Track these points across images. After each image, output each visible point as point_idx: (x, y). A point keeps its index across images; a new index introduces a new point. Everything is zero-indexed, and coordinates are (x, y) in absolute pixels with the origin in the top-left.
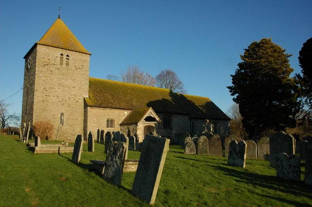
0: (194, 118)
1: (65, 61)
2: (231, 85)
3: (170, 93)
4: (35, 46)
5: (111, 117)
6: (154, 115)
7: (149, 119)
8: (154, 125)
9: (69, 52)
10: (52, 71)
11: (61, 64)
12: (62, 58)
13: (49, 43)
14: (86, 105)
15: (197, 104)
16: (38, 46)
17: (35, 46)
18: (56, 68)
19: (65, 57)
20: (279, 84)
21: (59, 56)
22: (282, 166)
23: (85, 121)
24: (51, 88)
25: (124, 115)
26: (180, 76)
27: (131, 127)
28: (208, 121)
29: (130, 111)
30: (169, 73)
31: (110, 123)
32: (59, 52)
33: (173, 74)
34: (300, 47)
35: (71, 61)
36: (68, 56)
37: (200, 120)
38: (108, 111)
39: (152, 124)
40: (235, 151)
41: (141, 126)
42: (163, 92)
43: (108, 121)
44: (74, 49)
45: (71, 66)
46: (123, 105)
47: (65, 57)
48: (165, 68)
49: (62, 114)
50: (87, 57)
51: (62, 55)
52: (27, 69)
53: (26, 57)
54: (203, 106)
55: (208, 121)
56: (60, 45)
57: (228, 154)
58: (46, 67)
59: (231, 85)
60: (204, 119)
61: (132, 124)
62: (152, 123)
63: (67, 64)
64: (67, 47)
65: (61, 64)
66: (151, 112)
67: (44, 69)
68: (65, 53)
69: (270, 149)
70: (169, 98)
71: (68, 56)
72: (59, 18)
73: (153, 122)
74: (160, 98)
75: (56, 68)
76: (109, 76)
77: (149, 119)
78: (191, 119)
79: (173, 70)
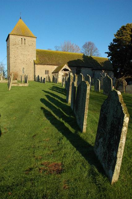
0: (94, 70)
1: (23, 42)
3: (83, 56)
4: (9, 35)
5: (47, 69)
6: (68, 68)
7: (65, 70)
8: (68, 73)
9: (25, 37)
11: (22, 44)
12: (22, 41)
13: (16, 34)
14: (35, 64)
15: (99, 62)
16: (10, 36)
17: (9, 35)
21: (21, 40)
23: (35, 71)
24: (17, 56)
25: (54, 68)
27: (56, 74)
28: (103, 71)
29: (57, 66)
30: (90, 43)
31: (47, 72)
32: (20, 38)
33: (93, 44)
34: (110, 39)
35: (26, 42)
36: (25, 39)
37: (99, 71)
38: (45, 66)
39: (67, 72)
41: (61, 74)
42: (79, 55)
43: (46, 71)
45: (27, 44)
46: (54, 63)
48: (87, 40)
49: (24, 68)
50: (35, 39)
51: (22, 39)
52: (7, 47)
53: (7, 41)
54: (102, 63)
55: (103, 71)
56: (20, 34)
58: (15, 46)
60: (101, 70)
61: (56, 72)
62: (66, 72)
63: (25, 43)
64: (24, 34)
65: (22, 44)
66: (66, 66)
67: (14, 47)
68: (23, 38)
69: (85, 106)
70: (82, 59)
71: (25, 39)
72: (21, 19)
73: (68, 72)
74: (76, 59)
76: (56, 46)
77: (65, 70)
78: (93, 70)
79: (92, 41)
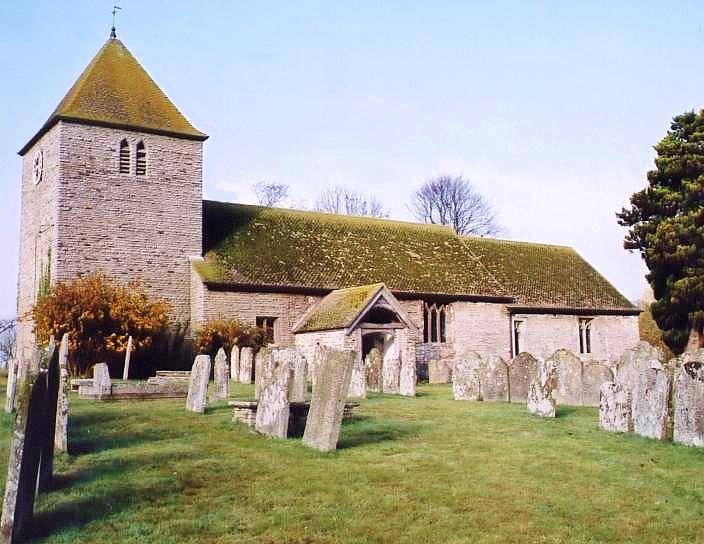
2: (648, 272)
10: (99, 191)
11: (123, 169)
12: (124, 154)
18: (112, 182)
19: (132, 149)
20: (410, 494)
21: (118, 147)
22: (607, 406)
26: (477, 179)
32: (115, 138)
40: (540, 383)
44: (155, 126)
47: (132, 149)
57: (103, 453)
58: (85, 180)
59: (648, 272)
63: (140, 169)
65: (123, 169)
68: (133, 139)
75: (112, 182)
